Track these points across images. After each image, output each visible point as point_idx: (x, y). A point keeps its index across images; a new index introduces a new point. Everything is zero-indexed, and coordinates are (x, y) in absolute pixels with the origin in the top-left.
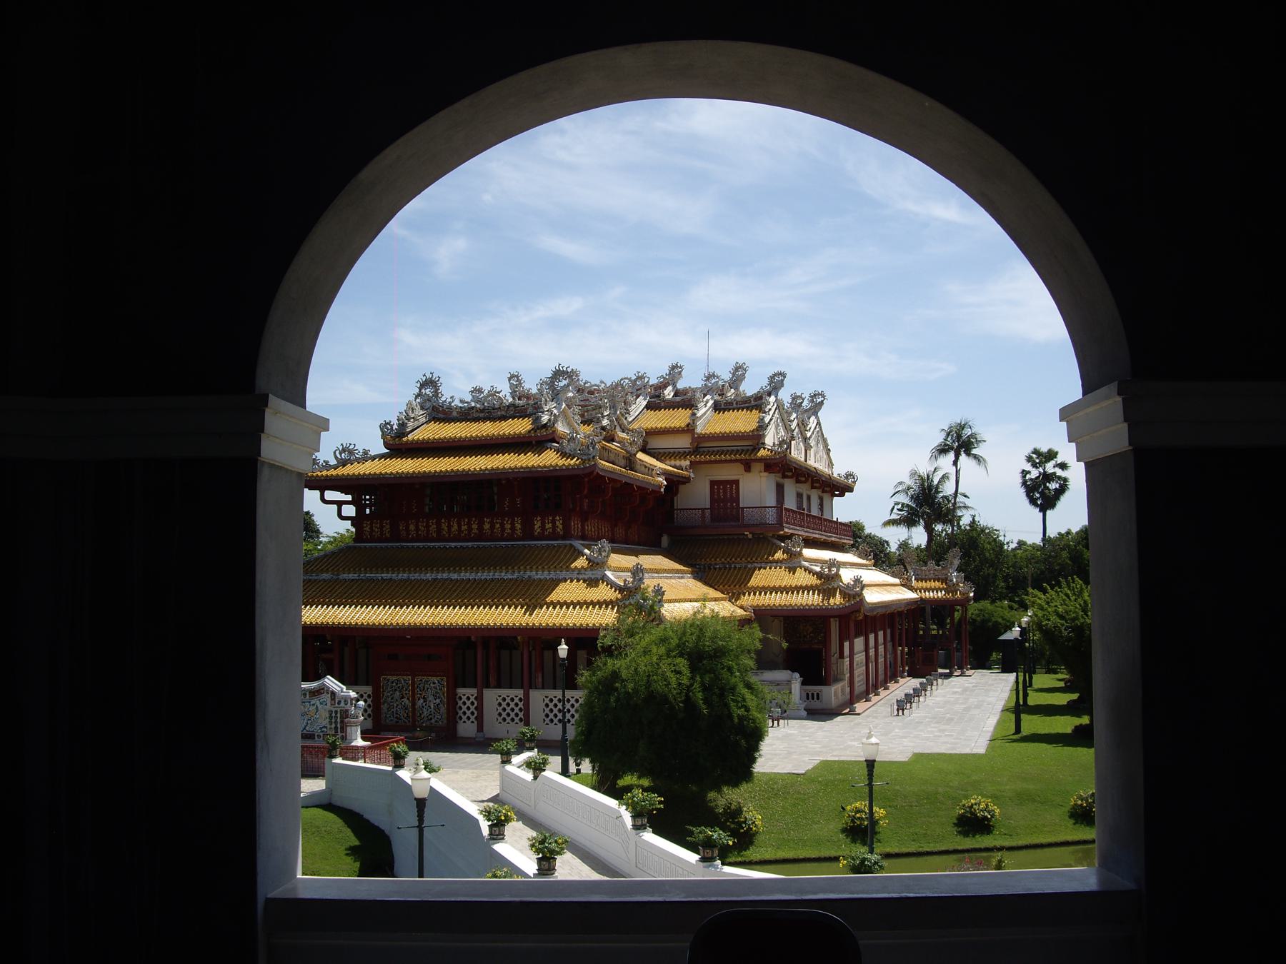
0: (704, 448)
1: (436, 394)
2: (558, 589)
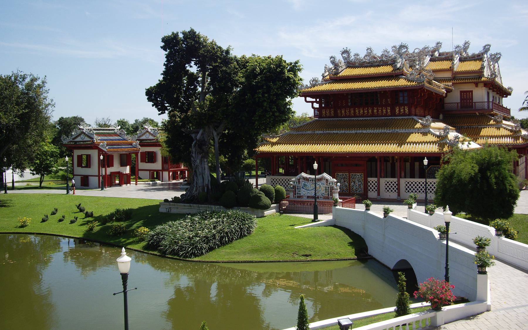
0: (457, 77)
1: (349, 56)
2: (410, 137)
